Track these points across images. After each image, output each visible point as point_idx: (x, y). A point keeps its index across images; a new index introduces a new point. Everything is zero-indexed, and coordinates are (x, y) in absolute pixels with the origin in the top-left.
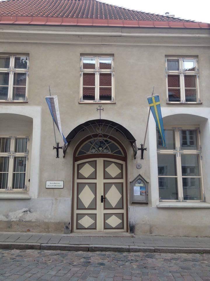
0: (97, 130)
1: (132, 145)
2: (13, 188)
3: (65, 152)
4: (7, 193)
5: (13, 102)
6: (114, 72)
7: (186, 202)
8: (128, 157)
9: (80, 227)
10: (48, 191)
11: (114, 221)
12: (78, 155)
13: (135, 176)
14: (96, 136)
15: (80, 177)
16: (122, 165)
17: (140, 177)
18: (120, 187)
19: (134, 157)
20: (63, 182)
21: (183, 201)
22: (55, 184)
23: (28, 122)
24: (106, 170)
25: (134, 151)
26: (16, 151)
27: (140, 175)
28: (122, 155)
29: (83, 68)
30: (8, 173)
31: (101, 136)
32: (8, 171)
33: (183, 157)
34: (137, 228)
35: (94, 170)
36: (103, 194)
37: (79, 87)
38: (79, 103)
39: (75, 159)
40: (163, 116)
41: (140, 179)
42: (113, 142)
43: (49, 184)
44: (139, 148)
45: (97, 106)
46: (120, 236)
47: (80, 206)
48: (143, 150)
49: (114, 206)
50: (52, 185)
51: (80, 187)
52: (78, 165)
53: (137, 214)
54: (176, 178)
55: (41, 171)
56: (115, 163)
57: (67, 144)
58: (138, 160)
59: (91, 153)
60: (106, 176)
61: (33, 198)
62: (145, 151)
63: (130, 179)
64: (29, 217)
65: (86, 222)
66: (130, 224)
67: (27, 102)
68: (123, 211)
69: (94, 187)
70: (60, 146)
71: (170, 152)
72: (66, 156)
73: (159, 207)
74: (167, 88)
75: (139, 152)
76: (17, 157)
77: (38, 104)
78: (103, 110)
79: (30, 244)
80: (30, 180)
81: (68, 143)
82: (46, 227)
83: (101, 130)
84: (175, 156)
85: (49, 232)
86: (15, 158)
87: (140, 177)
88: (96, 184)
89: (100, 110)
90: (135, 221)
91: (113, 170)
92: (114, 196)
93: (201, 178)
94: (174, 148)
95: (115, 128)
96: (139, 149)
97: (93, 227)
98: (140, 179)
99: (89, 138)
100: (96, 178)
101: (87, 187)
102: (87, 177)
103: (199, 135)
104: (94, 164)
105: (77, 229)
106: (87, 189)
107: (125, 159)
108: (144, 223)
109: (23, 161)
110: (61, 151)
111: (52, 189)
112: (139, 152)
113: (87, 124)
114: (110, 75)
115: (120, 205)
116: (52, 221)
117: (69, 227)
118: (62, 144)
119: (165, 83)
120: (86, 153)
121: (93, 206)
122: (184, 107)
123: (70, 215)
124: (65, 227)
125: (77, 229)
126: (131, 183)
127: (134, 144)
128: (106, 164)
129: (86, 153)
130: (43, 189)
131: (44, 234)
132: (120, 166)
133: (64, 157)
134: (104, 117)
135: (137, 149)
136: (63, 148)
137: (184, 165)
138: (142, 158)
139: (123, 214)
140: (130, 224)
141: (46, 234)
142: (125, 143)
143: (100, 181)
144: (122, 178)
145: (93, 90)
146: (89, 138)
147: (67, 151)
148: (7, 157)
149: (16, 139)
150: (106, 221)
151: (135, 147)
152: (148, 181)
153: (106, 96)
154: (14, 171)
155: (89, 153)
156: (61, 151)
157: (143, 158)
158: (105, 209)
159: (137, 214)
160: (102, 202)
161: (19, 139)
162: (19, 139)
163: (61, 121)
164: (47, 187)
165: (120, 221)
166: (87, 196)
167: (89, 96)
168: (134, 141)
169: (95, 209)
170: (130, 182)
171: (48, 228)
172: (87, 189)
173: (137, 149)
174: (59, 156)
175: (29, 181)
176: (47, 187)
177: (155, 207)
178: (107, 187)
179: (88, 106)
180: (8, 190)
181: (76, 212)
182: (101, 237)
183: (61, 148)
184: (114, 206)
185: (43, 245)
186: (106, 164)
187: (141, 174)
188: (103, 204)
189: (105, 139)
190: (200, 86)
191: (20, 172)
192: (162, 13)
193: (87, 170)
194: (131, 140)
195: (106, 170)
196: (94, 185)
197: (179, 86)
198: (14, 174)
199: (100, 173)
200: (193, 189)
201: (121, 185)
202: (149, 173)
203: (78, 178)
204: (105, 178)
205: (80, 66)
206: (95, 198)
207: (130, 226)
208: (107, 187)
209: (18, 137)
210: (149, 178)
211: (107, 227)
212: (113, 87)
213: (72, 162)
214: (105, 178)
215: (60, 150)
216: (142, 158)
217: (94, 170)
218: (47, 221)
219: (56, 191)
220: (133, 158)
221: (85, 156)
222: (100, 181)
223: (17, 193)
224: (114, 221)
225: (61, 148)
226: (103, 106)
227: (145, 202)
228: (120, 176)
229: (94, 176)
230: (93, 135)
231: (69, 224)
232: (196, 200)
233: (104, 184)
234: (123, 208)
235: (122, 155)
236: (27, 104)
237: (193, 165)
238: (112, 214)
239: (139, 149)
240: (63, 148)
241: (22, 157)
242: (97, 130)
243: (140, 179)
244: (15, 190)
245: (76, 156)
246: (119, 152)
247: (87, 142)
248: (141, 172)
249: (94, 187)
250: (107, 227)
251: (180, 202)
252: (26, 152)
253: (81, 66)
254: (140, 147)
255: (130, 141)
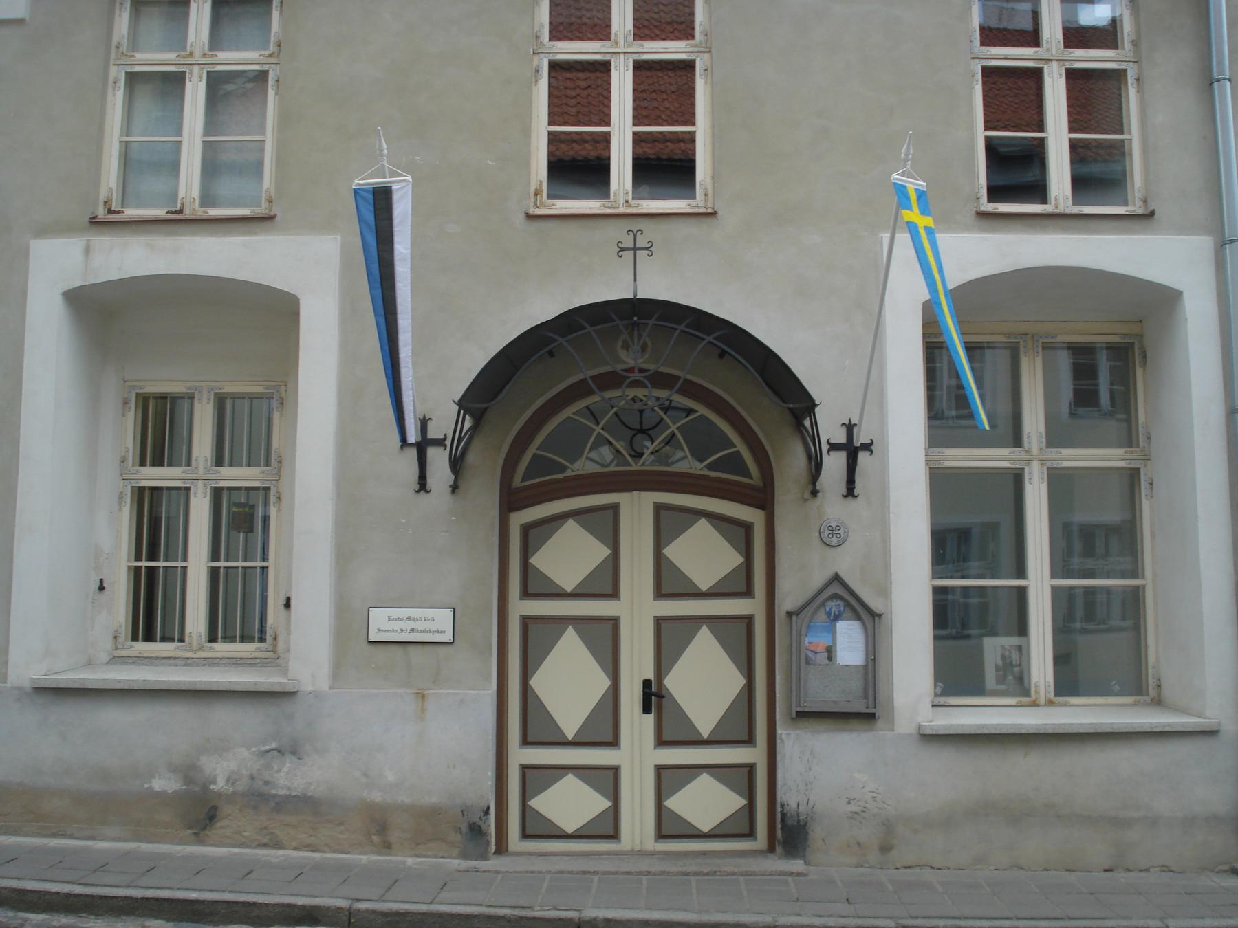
0: (623, 354)
1: (799, 425)
2: (212, 638)
3: (457, 464)
4: (187, 662)
5: (205, 216)
6: (707, 56)
7: (1065, 705)
8: (776, 484)
9: (538, 829)
10: (381, 654)
11: (707, 803)
12: (524, 479)
13: (818, 578)
14: (610, 381)
15: (535, 586)
16: (748, 528)
17: (835, 589)
18: (738, 638)
19: (810, 487)
20: (449, 612)
21: (1050, 703)
22: (411, 625)
23: (276, 313)
24: (668, 551)
25: (809, 457)
26: (219, 462)
27: (837, 578)
28: (751, 478)
29: (552, 38)
30: (184, 564)
31: (636, 384)
32: (185, 559)
33: (1060, 482)
34: (816, 833)
35: (606, 552)
36: (650, 675)
37: (527, 133)
38: (529, 217)
39: (511, 501)
40: (950, 286)
41: (843, 599)
42: (702, 410)
43: (385, 622)
44: (832, 441)
45: (617, 232)
46: (736, 870)
47: (538, 728)
48: (852, 450)
49: (705, 728)
50: (397, 625)
51: (537, 639)
52: (526, 529)
53: (822, 770)
54: (1022, 593)
55: (344, 557)
56: (713, 517)
57: (468, 425)
58: (832, 505)
59: (597, 469)
60: (668, 582)
61: (310, 688)
62: (863, 457)
63: (788, 598)
64: (290, 778)
65: (571, 804)
66: (783, 815)
67: (272, 218)
68: (753, 755)
69: (605, 640)
70: (433, 433)
71: (997, 458)
72: (462, 485)
73: (928, 732)
74: (980, 135)
75: (834, 464)
76: (230, 489)
77: (326, 226)
78: (647, 249)
79: (300, 901)
80: (288, 599)
81: (472, 416)
82: (379, 825)
83: (644, 349)
84: (1017, 479)
85: (387, 847)
86: (217, 493)
87: (835, 589)
88: (615, 621)
89: (635, 249)
90: (811, 803)
91: (704, 555)
92: (706, 682)
93: (1144, 586)
94: (1016, 439)
95: (710, 342)
96: (834, 447)
97: (606, 828)
98: (835, 596)
99: (579, 391)
100: (614, 594)
101: (570, 635)
102: (569, 590)
103: (1139, 372)
104: (606, 525)
105: (525, 835)
106: (570, 645)
107: (763, 498)
108: (852, 808)
109: (253, 507)
110: (439, 460)
111: (399, 650)
112: (834, 464)
113: (570, 322)
114: (687, 67)
115: (739, 725)
116: (404, 798)
117: (477, 834)
118: (444, 421)
119: (971, 110)
120: (564, 469)
121: (604, 728)
122: (1065, 230)
123: (490, 773)
124: (465, 829)
125: (525, 835)
126: (794, 617)
127: (807, 423)
128: (668, 525)
129: (657, 320)
130: (354, 645)
131: (364, 858)
132: (740, 534)
133: (454, 488)
134: (657, 285)
135: (825, 447)
136: (448, 442)
137: (1023, 639)
138: (850, 492)
139: (751, 768)
140: (783, 815)
141: (374, 858)
142: (763, 413)
143: (637, 610)
144: (748, 593)
145: (642, 87)
146: (579, 391)
147: (471, 458)
148: (178, 488)
149: (221, 401)
150: (705, 733)
151: (815, 437)
152: (875, 604)
153: (665, 167)
154: (215, 556)
155: (583, 467)
156: (439, 460)
157: (856, 492)
158: (661, 742)
159: (822, 770)
160: (647, 709)
161: (234, 398)
162: (234, 398)
163: (414, 353)
164: (372, 638)
165: (738, 802)
166: (569, 683)
167: (578, 167)
168: (808, 406)
169: (614, 743)
170: (790, 614)
171: (382, 828)
172: (570, 645)
173: (825, 447)
174: (431, 481)
175: (287, 605)
176: (373, 637)
177: (910, 735)
178: (670, 639)
179: (572, 228)
180: (190, 648)
181: (519, 755)
182: (640, 873)
183: (440, 442)
184: (705, 728)
185: (362, 906)
186: (668, 525)
187: (842, 574)
188: (650, 718)
189: (663, 394)
190: (1151, 123)
191: (240, 564)
192: (184, 924)
193: (569, 556)
194: (796, 402)
195: (668, 551)
196: (609, 625)
197: (1041, 127)
198: (214, 574)
199: (639, 558)
200: (1105, 636)
201: (742, 626)
202: (887, 568)
203: (526, 594)
204: (660, 594)
205: (536, 29)
206: (614, 691)
207: (783, 820)
208: (670, 639)
209: (229, 388)
210: (884, 591)
211: (668, 827)
212: (702, 129)
213: (495, 513)
214: (660, 594)
215: (432, 452)
216: (850, 492)
217: (606, 552)
218: (377, 796)
219: (415, 654)
220: (807, 495)
221: (559, 481)
222: (637, 610)
223: (229, 666)
224: (707, 803)
225: (440, 442)
226: (650, 231)
227: (859, 707)
228: (738, 584)
229: (605, 582)
230: (590, 392)
231: (487, 812)
232: (1117, 695)
233: (659, 622)
234: (750, 741)
235: (751, 478)
236: (268, 224)
237: (1112, 515)
238: (694, 770)
239: (834, 447)
240: (448, 442)
241: (248, 489)
242: (623, 354)
243: (835, 596)
244: (222, 649)
245: (517, 482)
246: (734, 464)
247: (569, 412)
248: (845, 563)
249: (605, 640)
250: (668, 827)
251: (1035, 704)
252: (268, 464)
253: (542, 26)
254: (841, 438)
255: (790, 409)
